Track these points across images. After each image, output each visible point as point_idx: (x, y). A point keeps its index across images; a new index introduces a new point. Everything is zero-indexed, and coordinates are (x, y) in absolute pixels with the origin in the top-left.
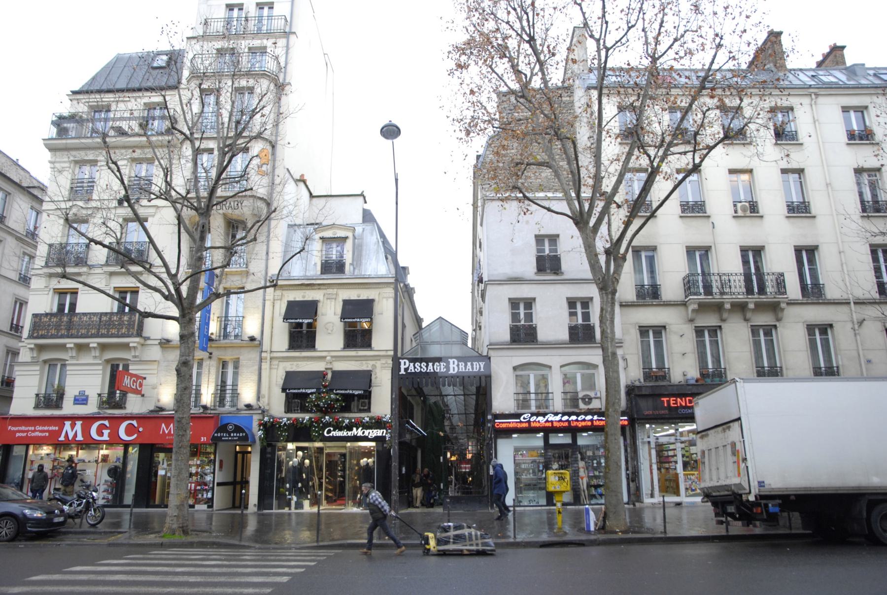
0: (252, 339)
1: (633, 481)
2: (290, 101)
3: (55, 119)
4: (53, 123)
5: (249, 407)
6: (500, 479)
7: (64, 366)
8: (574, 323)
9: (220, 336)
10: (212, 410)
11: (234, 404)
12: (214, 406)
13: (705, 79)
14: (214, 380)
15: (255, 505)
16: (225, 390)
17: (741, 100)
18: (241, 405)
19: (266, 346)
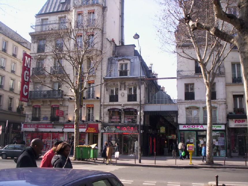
0: (98, 98)
1: (228, 149)
2: (119, 2)
3: (36, 15)
4: (38, 15)
5: (97, 121)
6: (24, 142)
7: (40, 108)
8: (130, 94)
9: (87, 98)
10: (86, 122)
11: (92, 120)
12: (86, 121)
13: (82, 11)
14: (86, 112)
15: (100, 153)
16: (90, 116)
17: (67, 22)
18: (95, 121)
19: (102, 100)
